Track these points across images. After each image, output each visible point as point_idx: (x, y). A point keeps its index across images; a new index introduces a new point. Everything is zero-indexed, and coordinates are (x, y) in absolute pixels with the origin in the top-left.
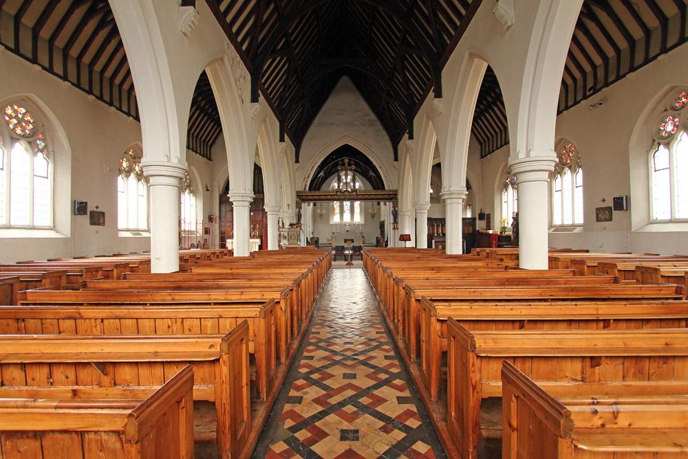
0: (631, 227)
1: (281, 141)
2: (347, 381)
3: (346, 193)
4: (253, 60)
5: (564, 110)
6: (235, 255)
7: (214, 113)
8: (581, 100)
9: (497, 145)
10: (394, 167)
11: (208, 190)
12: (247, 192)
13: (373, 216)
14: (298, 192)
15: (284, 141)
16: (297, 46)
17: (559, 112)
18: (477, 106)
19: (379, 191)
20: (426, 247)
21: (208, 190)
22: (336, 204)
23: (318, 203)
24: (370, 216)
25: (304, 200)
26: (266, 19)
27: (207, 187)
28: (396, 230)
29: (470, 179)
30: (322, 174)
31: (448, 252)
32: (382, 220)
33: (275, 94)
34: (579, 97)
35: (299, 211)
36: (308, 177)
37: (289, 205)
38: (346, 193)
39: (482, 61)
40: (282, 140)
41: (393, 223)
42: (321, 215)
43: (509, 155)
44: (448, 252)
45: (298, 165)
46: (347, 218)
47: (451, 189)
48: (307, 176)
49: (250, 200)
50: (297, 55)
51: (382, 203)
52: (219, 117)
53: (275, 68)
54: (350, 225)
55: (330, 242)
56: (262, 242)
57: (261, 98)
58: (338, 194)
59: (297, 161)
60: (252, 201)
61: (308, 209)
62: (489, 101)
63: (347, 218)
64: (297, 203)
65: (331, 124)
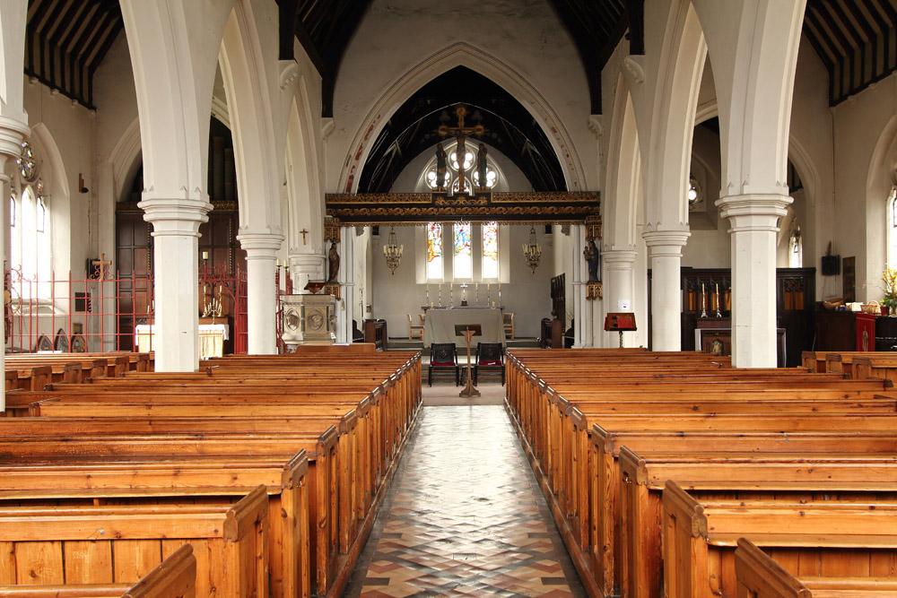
1: (324, 115)
3: (461, 201)
6: (159, 368)
10: (593, 130)
11: (84, 190)
13: (534, 262)
14: (329, 197)
19: (550, 197)
21: (84, 190)
22: (434, 231)
23: (385, 229)
24: (529, 261)
25: (346, 219)
27: (81, 182)
29: (799, 164)
30: (394, 147)
32: (558, 273)
35: (334, 248)
36: (358, 157)
37: (304, 232)
42: (393, 261)
45: (330, 122)
46: (463, 266)
48: (353, 154)
54: (471, 287)
55: (416, 332)
59: (327, 112)
60: (206, 219)
61: (357, 242)
64: (327, 225)
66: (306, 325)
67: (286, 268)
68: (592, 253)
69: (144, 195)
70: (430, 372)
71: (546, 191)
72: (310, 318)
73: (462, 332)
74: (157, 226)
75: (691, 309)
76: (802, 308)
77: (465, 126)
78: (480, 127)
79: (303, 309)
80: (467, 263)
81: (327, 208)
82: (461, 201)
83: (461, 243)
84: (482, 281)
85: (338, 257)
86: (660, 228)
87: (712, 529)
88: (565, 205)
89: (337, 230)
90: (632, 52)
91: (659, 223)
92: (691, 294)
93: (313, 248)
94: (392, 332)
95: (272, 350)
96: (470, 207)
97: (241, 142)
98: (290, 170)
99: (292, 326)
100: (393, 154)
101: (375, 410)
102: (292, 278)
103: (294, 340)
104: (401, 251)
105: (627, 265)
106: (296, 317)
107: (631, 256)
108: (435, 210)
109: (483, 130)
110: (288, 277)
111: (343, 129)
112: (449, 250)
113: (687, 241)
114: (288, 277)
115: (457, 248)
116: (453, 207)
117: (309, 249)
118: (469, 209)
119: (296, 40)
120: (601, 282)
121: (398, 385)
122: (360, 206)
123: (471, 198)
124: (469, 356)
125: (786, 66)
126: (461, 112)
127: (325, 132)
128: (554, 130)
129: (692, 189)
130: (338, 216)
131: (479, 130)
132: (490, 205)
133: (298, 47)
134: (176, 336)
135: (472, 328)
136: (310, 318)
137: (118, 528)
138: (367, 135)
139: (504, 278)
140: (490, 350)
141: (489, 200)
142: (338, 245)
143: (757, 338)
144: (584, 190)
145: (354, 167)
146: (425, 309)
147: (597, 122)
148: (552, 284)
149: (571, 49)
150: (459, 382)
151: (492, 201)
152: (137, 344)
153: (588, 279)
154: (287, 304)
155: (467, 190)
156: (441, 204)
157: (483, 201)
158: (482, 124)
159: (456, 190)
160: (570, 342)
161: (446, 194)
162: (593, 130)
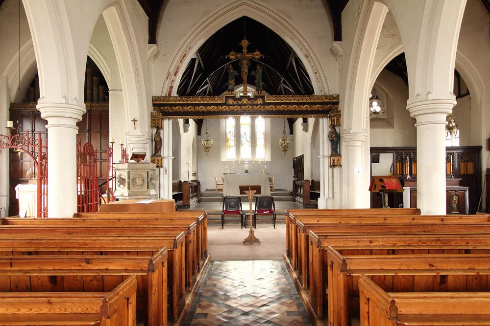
0: (303, 178)
1: (150, 42)
2: (241, 284)
3: (245, 101)
10: (334, 53)
13: (285, 149)
14: (154, 99)
24: (282, 146)
25: (167, 114)
28: (336, 169)
29: (473, 79)
32: (298, 154)
35: (158, 133)
36: (175, 75)
37: (134, 121)
38: (245, 101)
39: (383, 5)
41: (331, 156)
42: (207, 148)
43: (407, 98)
45: (154, 46)
46: (246, 152)
48: (172, 70)
49: (76, 116)
54: (250, 162)
55: (220, 187)
58: (230, 101)
59: (153, 40)
63: (246, 152)
64: (153, 117)
66: (131, 185)
67: (122, 145)
68: (334, 136)
70: (223, 216)
71: (302, 94)
72: (134, 179)
73: (245, 192)
75: (398, 174)
76: (472, 173)
77: (247, 52)
78: (258, 53)
79: (129, 173)
81: (153, 106)
84: (256, 160)
87: (400, 311)
91: (351, 129)
92: (398, 164)
93: (141, 132)
94: (203, 190)
96: (251, 105)
97: (31, 16)
98: (123, 76)
99: (121, 185)
100: (208, 90)
103: (122, 196)
104: (212, 143)
105: (359, 143)
106: (124, 180)
107: (362, 138)
108: (227, 107)
109: (260, 55)
111: (165, 55)
113: (454, 109)
115: (243, 143)
116: (239, 105)
117: (138, 132)
118: (250, 107)
120: (340, 155)
123: (252, 99)
124: (251, 205)
125: (459, 19)
127: (151, 55)
129: (378, 105)
131: (256, 55)
135: (253, 188)
136: (134, 179)
138: (182, 60)
139: (376, 5)
140: (265, 202)
141: (264, 100)
142: (161, 131)
144: (327, 93)
145: (173, 81)
146: (225, 174)
147: (339, 48)
148: (294, 161)
150: (244, 225)
151: (266, 102)
152: (17, 198)
153: (330, 154)
154: (118, 169)
155: (249, 94)
156: (231, 103)
158: (259, 51)
159: (242, 94)
161: (235, 97)
162: (334, 53)
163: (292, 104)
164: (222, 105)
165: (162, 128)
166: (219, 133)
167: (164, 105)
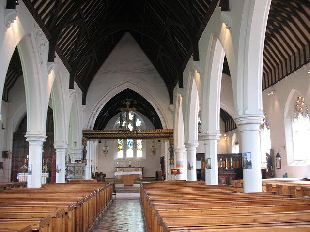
1: (83, 105)
4: (52, 31)
5: (286, 76)
6: (29, 186)
7: (18, 68)
8: (303, 65)
9: (287, 71)
10: (170, 110)
11: (4, 128)
12: (42, 133)
13: (154, 152)
15: (73, 88)
16: (86, 17)
17: (263, 90)
18: (270, 22)
19: (157, 132)
20: (217, 183)
21: (4, 128)
22: (120, 142)
23: (103, 141)
24: (151, 151)
25: (89, 138)
26: (64, 3)
27: (3, 125)
30: (107, 113)
31: (207, 183)
33: (67, 52)
34: (302, 63)
35: (85, 147)
40: (71, 87)
44: (207, 183)
45: (85, 106)
46: (130, 153)
47: (208, 132)
50: (87, 22)
51: (162, 141)
52: (22, 70)
53: (69, 34)
56: (50, 176)
57: (57, 58)
58: (121, 132)
59: (84, 104)
60: (45, 141)
61: (92, 145)
62: (275, 26)
63: (130, 153)
64: (83, 140)
65: (115, 72)
69: (27, 133)
72: (77, 171)
74: (30, 143)
80: (133, 152)
82: (128, 132)
83: (129, 145)
85: (86, 151)
86: (189, 142)
88: (162, 133)
89: (86, 142)
90: (180, 88)
95: (64, 181)
97: (28, 92)
101: (95, 197)
102: (71, 157)
106: (72, 171)
110: (69, 157)
112: (125, 148)
114: (69, 157)
119: (75, 82)
121: (103, 191)
122: (94, 134)
126: (128, 104)
128: (159, 109)
130: (86, 137)
132: (137, 134)
133: (75, 85)
134: (35, 178)
137: (33, 215)
143: (213, 178)
149: (163, 84)
157: (135, 132)
160: (165, 179)
162: (170, 110)
163: (151, 134)
164: (116, 134)
165: (86, 145)
166: (23, 37)
167: (88, 134)
